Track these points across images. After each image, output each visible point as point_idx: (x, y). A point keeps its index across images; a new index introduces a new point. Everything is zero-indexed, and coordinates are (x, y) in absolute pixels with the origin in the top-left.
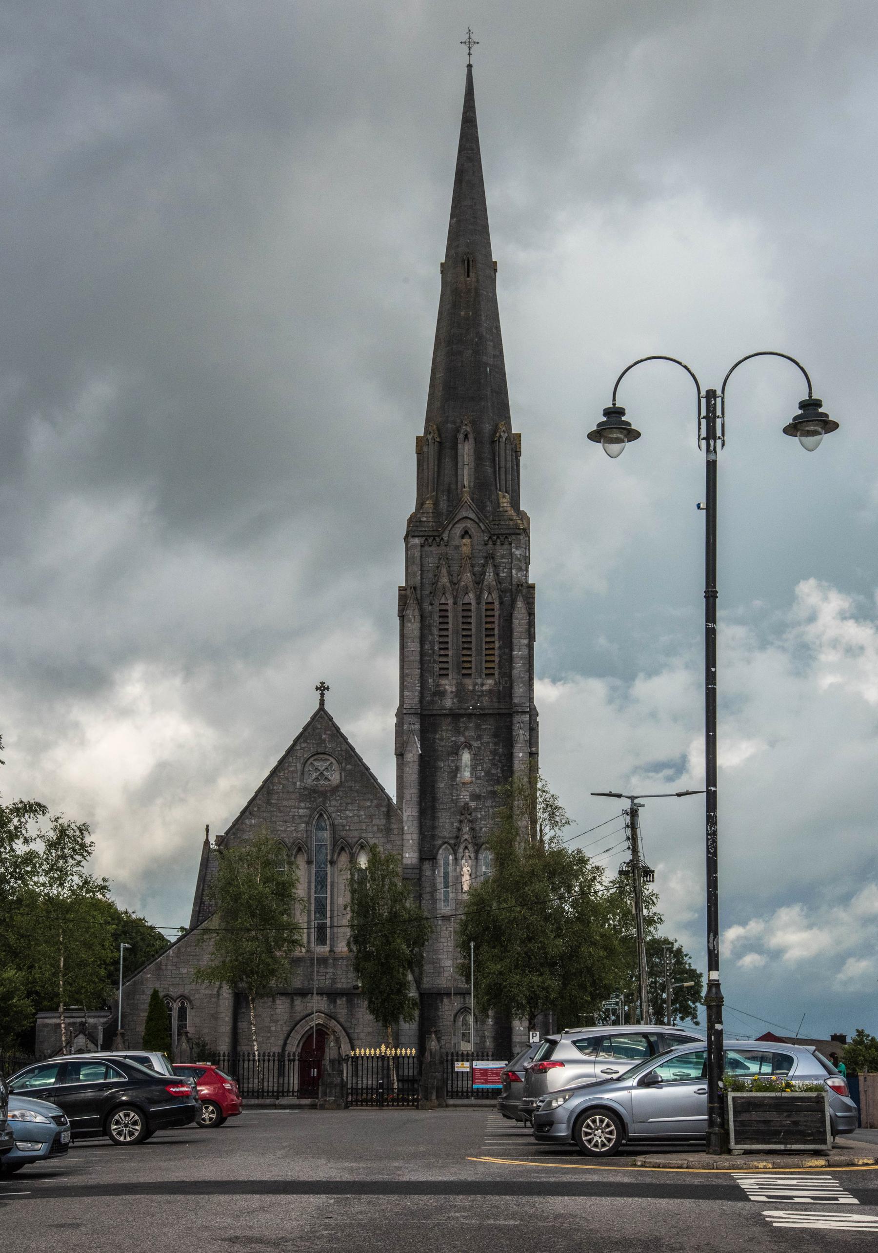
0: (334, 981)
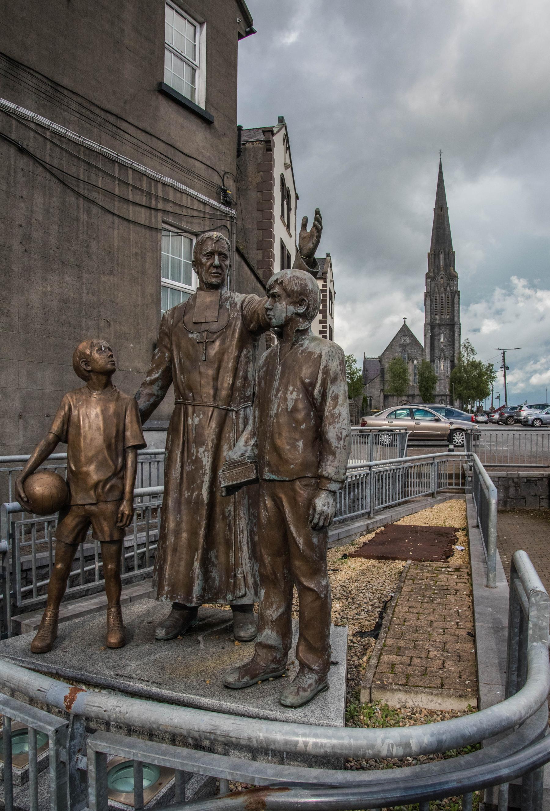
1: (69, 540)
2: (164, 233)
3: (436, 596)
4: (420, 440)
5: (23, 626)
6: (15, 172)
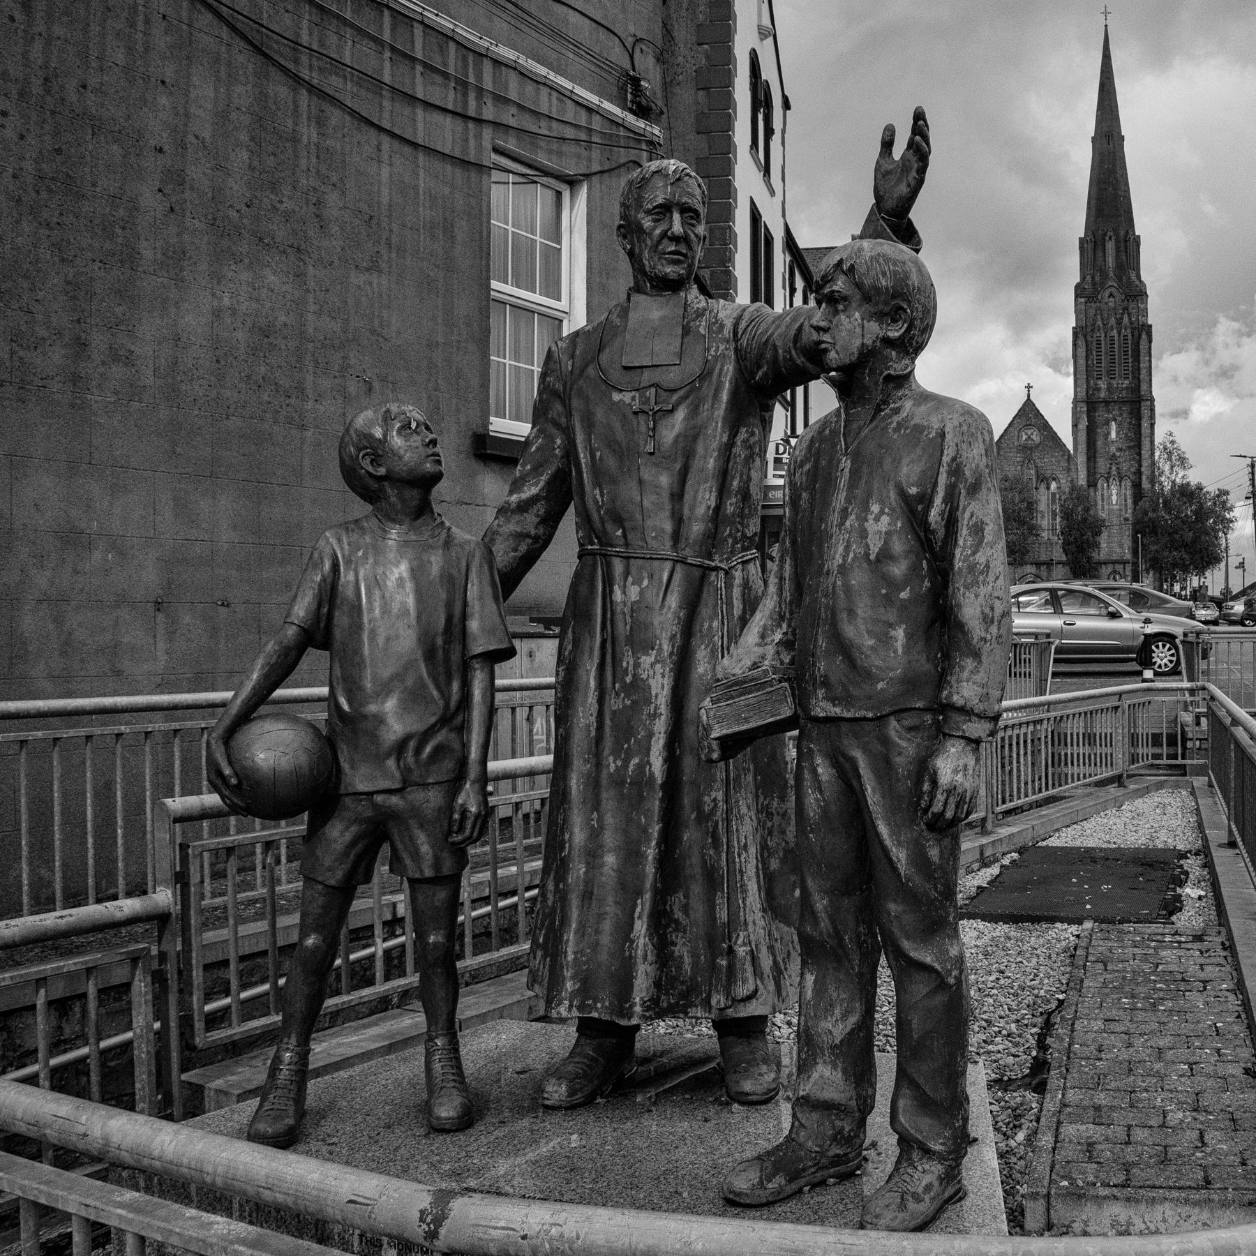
1: (335, 878)
2: (496, 176)
3: (1161, 994)
4: (1080, 660)
5: (209, 1096)
6: (147, 22)
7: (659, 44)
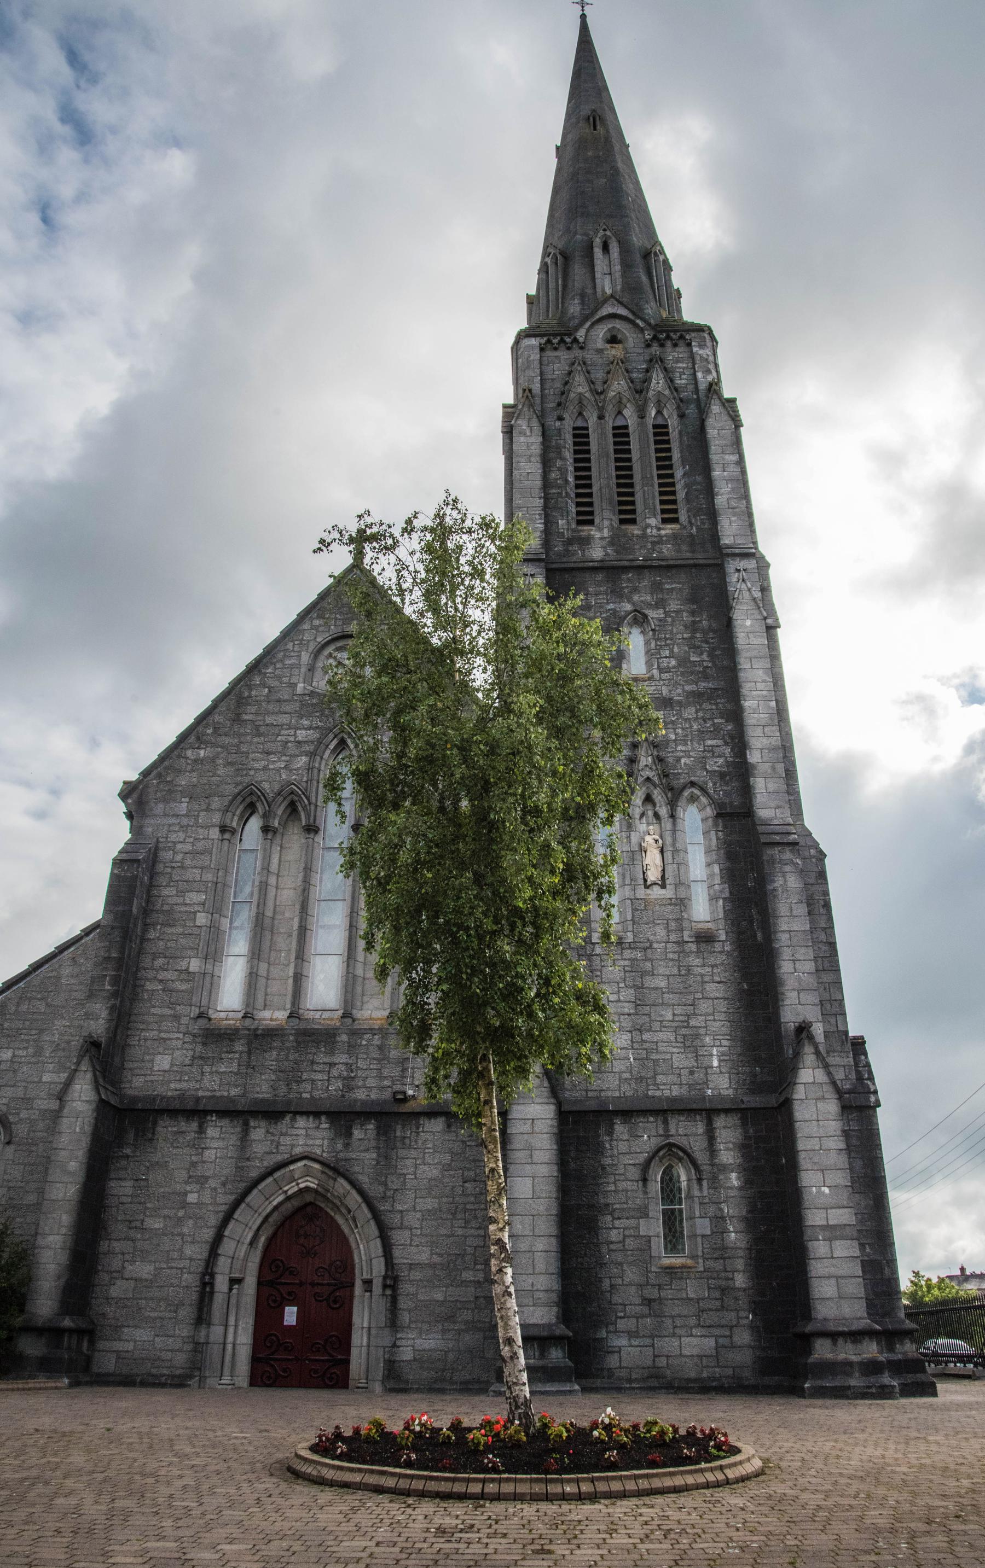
0: (349, 1083)
7: (831, 1069)
